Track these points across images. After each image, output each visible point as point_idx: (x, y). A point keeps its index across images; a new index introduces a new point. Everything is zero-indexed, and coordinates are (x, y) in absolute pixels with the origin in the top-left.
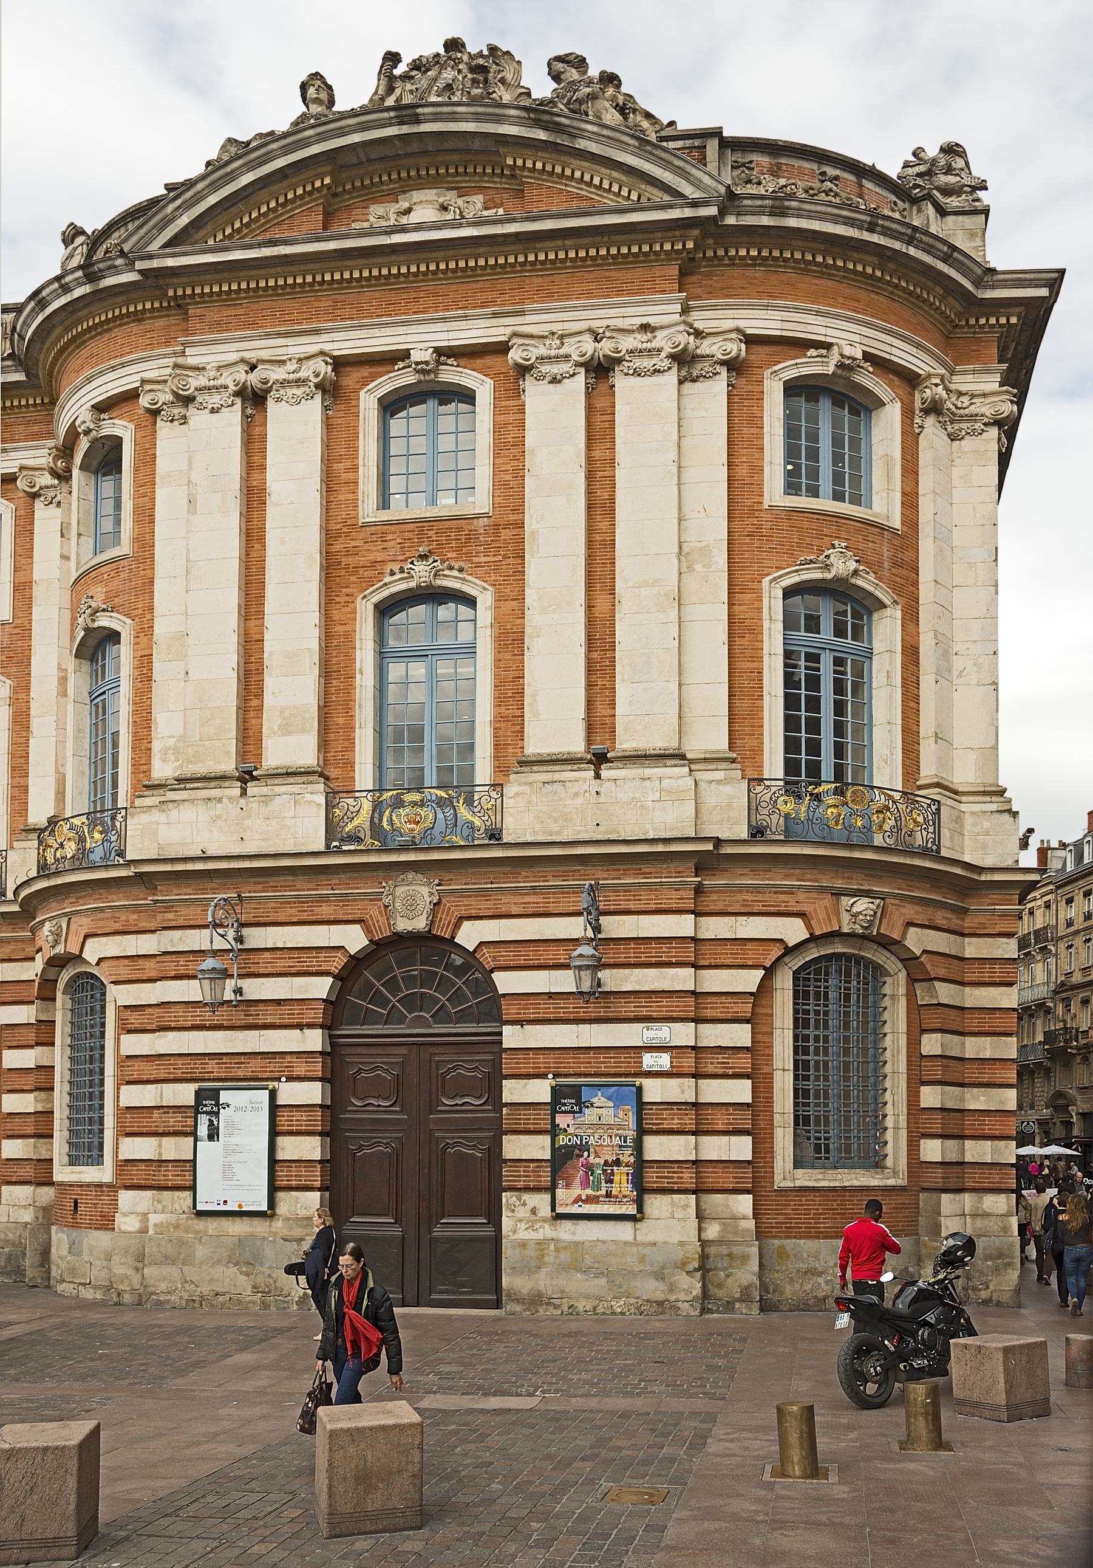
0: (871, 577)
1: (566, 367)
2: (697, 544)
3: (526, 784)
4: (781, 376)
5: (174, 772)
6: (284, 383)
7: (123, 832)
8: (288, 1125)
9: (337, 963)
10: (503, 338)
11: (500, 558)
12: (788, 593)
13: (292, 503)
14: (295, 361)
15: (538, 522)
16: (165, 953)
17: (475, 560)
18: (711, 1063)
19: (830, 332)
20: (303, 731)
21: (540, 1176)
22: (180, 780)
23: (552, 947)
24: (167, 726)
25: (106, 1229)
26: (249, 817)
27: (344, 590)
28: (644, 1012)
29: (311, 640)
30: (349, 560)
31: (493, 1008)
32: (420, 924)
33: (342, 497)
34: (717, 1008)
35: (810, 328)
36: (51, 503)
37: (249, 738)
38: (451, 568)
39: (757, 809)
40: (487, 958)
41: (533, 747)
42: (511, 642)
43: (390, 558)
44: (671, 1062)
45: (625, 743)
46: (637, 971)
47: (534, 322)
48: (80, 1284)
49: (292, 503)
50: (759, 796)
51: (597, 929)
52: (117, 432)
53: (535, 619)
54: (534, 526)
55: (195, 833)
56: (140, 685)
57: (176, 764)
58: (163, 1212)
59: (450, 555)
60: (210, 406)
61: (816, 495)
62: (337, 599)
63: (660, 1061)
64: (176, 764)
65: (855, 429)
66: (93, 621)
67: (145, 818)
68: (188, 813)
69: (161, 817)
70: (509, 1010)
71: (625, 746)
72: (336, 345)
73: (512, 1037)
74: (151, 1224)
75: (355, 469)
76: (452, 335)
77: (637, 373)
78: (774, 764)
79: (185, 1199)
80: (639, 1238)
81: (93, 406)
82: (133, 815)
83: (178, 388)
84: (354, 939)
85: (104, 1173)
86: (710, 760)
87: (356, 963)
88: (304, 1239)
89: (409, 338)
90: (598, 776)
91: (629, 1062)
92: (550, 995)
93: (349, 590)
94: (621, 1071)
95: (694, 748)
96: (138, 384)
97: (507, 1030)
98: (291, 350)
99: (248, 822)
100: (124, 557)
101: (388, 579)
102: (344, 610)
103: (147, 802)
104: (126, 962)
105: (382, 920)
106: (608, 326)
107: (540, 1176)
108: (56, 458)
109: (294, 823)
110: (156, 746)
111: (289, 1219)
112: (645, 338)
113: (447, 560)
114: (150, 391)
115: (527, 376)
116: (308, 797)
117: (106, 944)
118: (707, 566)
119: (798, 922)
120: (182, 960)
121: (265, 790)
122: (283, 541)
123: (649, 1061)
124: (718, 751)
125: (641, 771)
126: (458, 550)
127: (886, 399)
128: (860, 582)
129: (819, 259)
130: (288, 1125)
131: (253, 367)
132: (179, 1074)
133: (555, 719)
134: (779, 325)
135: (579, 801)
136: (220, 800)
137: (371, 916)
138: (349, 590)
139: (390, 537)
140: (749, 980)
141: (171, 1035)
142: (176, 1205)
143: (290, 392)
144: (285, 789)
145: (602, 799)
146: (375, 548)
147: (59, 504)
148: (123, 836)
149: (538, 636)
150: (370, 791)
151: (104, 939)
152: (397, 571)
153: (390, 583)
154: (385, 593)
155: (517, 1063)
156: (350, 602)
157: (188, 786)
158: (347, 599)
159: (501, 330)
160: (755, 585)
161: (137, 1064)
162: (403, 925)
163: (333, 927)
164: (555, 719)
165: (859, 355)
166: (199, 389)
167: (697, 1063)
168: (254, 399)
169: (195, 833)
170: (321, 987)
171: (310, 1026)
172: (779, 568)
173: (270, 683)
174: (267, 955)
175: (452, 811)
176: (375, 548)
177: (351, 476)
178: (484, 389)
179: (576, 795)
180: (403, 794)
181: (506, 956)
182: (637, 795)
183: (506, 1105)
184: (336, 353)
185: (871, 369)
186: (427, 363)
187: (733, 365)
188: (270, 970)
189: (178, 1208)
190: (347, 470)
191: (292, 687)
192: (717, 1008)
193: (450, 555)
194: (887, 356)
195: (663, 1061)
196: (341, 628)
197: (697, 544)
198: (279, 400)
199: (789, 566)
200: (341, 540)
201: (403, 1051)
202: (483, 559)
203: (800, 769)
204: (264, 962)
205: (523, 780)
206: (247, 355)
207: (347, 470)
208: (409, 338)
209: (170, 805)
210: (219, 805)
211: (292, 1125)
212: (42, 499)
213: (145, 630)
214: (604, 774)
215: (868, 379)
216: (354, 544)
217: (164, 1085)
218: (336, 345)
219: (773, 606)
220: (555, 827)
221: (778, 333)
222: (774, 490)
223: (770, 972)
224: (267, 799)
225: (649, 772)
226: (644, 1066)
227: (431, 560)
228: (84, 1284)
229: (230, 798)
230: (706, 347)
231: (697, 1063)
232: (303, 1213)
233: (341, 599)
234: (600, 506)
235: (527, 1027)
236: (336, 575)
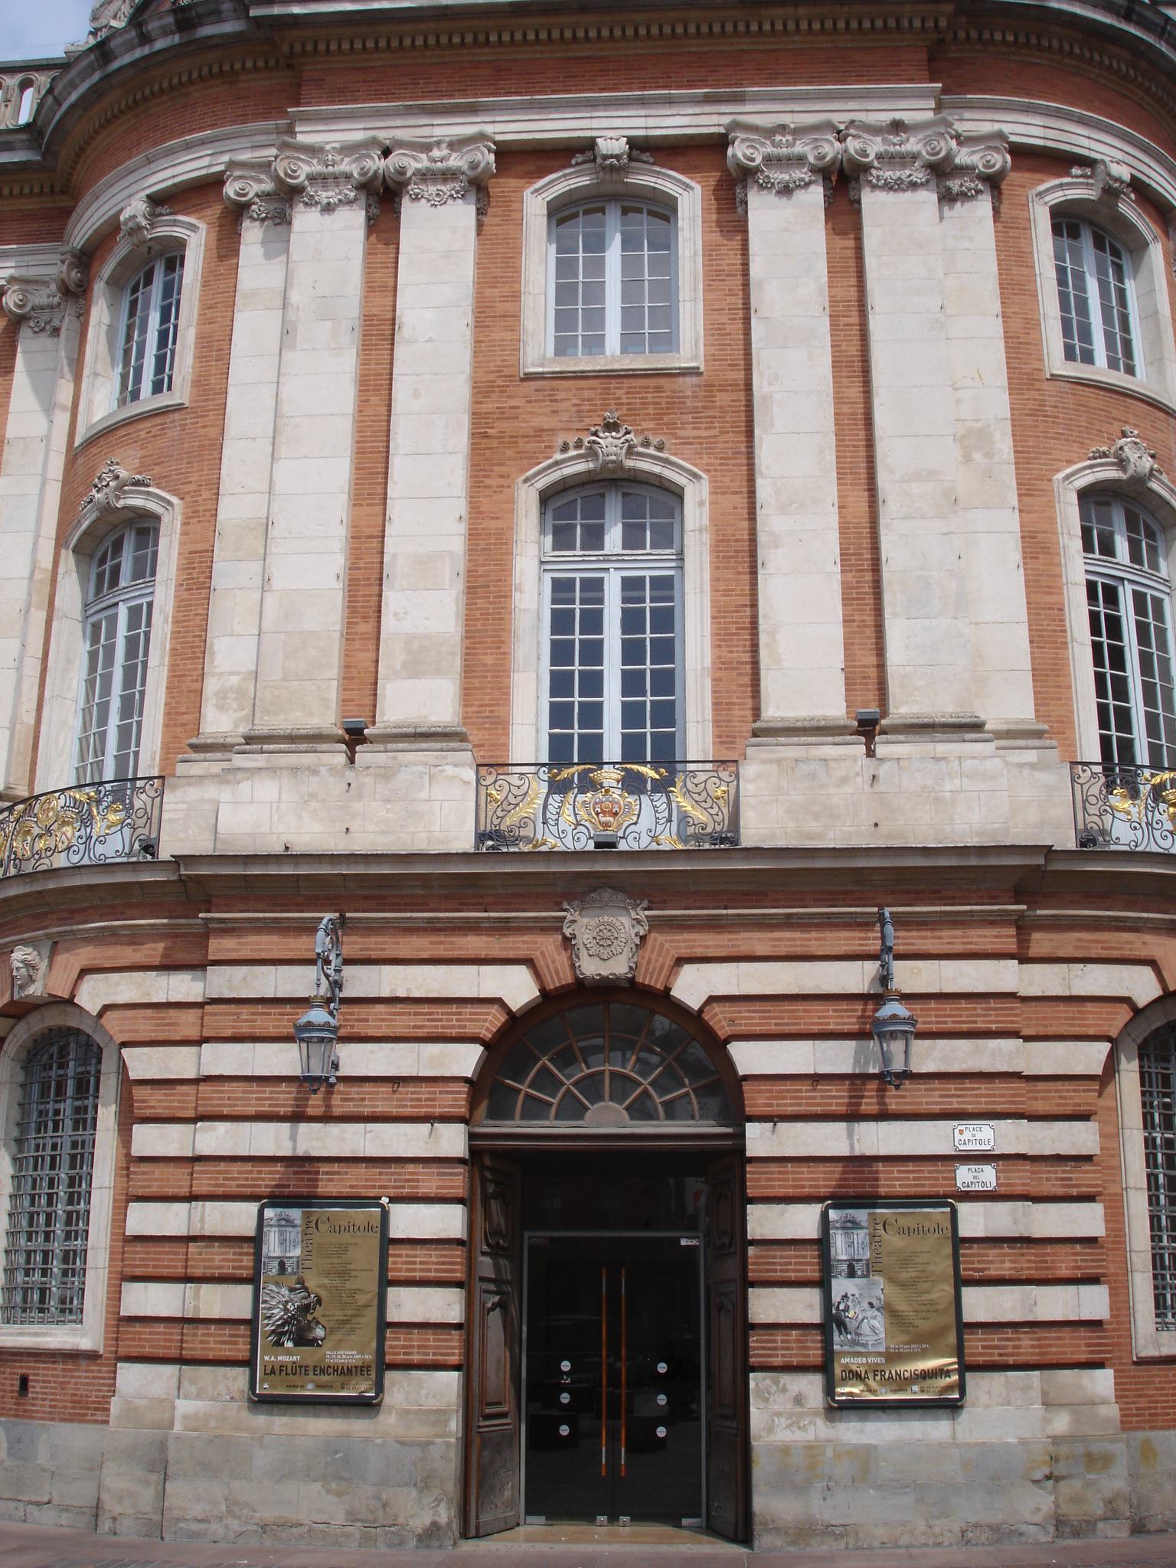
1: (800, 174)
2: (975, 425)
3: (771, 761)
4: (1047, 199)
5: (236, 726)
6: (425, 176)
7: (156, 813)
8: (407, 1270)
9: (490, 1022)
10: (722, 130)
11: (715, 432)
12: (1084, 495)
13: (431, 340)
14: (444, 146)
15: (770, 384)
16: (214, 1001)
17: (680, 433)
18: (1048, 1180)
19: (1094, 145)
20: (438, 672)
21: (807, 1348)
22: (249, 739)
23: (817, 1006)
24: (229, 656)
25: (80, 1422)
26: (360, 797)
27: (496, 469)
28: (955, 1105)
29: (453, 540)
30: (505, 425)
31: (728, 1094)
32: (618, 967)
33: (496, 336)
34: (1053, 1098)
35: (1074, 139)
36: (43, 330)
37: (362, 679)
38: (646, 444)
39: (1085, 809)
40: (720, 1021)
41: (774, 710)
42: (742, 555)
43: (561, 425)
44: (998, 1178)
45: (903, 707)
46: (941, 1043)
47: (759, 113)
48: (30, 1503)
49: (431, 340)
50: (1085, 787)
52: (179, 232)
53: (771, 522)
54: (766, 389)
55: (275, 818)
56: (186, 595)
57: (239, 714)
58: (198, 1397)
59: (645, 425)
60: (325, 201)
62: (488, 482)
63: (982, 1177)
64: (239, 714)
65: (657, 265)
66: (118, 498)
67: (192, 793)
68: (266, 790)
69: (225, 794)
70: (756, 1100)
71: (903, 710)
72: (499, 128)
73: (758, 1139)
74: (178, 1414)
75: (516, 296)
76: (651, 122)
77: (888, 187)
79: (235, 1379)
80: (454, 1359)
81: (148, 196)
82: (174, 788)
83: (286, 174)
84: (517, 988)
85: (85, 1335)
86: (1012, 735)
87: (516, 1022)
88: (432, 1443)
89: (595, 123)
90: (870, 753)
91: (937, 1179)
92: (816, 1078)
93: (504, 470)
94: (931, 1190)
95: (994, 717)
96: (222, 168)
97: (752, 1130)
98: (438, 132)
99: (358, 806)
100: (179, 408)
101: (559, 456)
102: (496, 497)
103: (196, 769)
104: (149, 1012)
105: (561, 959)
106: (853, 122)
107: (807, 1348)
108: (72, 266)
109: (432, 812)
110: (211, 686)
111: (407, 1412)
112: (896, 140)
113: (642, 431)
114: (240, 177)
115: (750, 181)
116: (450, 770)
117: (118, 984)
118: (989, 455)
119: (1147, 972)
120: (245, 1011)
121: (382, 758)
122: (416, 394)
123: (965, 1176)
124: (1023, 721)
125: (930, 746)
126: (657, 418)
127: (1149, 238)
128: (1154, 485)
129: (1077, 50)
130: (407, 1270)
131: (386, 153)
132: (232, 1188)
133: (805, 671)
134: (1040, 132)
135: (848, 789)
136: (315, 772)
137: (542, 953)
138: (504, 470)
139: (561, 396)
141: (222, 1127)
142: (221, 1388)
143: (432, 189)
144: (415, 760)
145: (880, 787)
146: (541, 411)
147: (56, 331)
148: (155, 820)
149: (777, 547)
150: (543, 765)
151: (116, 976)
152: (571, 445)
153: (563, 461)
154: (555, 476)
155: (768, 1179)
156: (505, 485)
157: (265, 747)
158: (502, 481)
159: (715, 119)
160: (1044, 485)
161: (158, 1170)
162: (591, 968)
163: (484, 969)
164: (805, 671)
165: (1127, 178)
166: (312, 178)
167: (1031, 1178)
168: (383, 199)
169: (275, 818)
170: (465, 1060)
171: (445, 1119)
172: (1070, 462)
173: (393, 599)
174: (380, 1008)
175: (664, 799)
176: (541, 411)
177: (508, 307)
178: (691, 198)
179: (844, 780)
180: (592, 771)
181: (749, 1018)
182: (930, 783)
183: (753, 1242)
184: (499, 138)
185: (1133, 196)
186: (618, 157)
187: (993, 182)
188: (383, 1031)
189: (224, 1392)
190: (504, 299)
191: (424, 609)
192: (1053, 1098)
193: (645, 425)
194: (1147, 180)
195: (987, 1177)
196: (493, 524)
197: (975, 425)
198: (416, 198)
199: (1081, 460)
200: (495, 397)
202: (690, 433)
204: (376, 1020)
205: (764, 756)
206: (382, 135)
207: (504, 299)
208: (595, 123)
209: (240, 775)
210: (314, 779)
211: (414, 1270)
212: (32, 324)
213: (204, 512)
214: (881, 750)
215: (1128, 209)
216: (512, 403)
217: (208, 1204)
218: (499, 128)
219: (1069, 516)
220: (814, 826)
221: (1041, 142)
222: (1055, 361)
224: (386, 774)
225: (942, 748)
226: (959, 1184)
227: (623, 431)
228: (38, 1504)
229: (332, 769)
230: (964, 156)
231: (1031, 1178)
232: (430, 1403)
233: (493, 482)
235: (783, 1126)
236: (492, 448)
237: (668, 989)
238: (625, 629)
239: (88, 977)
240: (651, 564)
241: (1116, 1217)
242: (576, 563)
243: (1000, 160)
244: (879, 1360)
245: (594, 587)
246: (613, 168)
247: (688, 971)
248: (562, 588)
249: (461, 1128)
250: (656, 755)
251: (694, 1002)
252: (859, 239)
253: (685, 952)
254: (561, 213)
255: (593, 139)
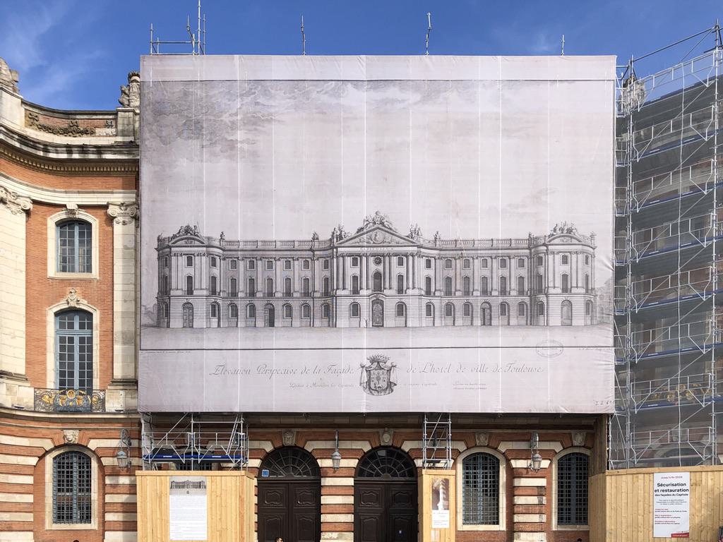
0: (85, 302)
51: (130, 444)
61: (73, 271)
78: (52, 381)
119: (49, 441)
140: (33, 461)
170: (353, 463)
171: (350, 477)
201: (381, 486)
203: (65, 382)
215: (82, 215)
222: (52, 270)
223: (42, 458)
234: (413, 274)
237: (400, 447)
239: (308, 442)
240: (85, 333)
243: (29, 206)
245: (71, 340)
246: (72, 212)
247: (92, 441)
248: (62, 340)
249: (353, 479)
251: (310, 450)
253: (91, 436)
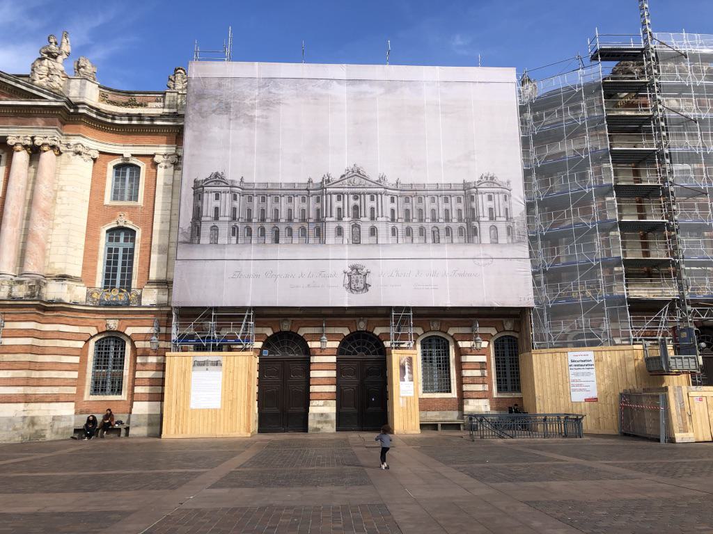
84: (346, 332)
119: (95, 328)
170: (336, 344)
238: (123, 258)
240: (129, 245)
241: (489, 359)
242: (114, 245)
244: (604, 360)
245: (117, 250)
247: (128, 328)
248: (110, 250)
250: (126, 284)
251: (377, 334)
252: (157, 170)
254: (117, 167)
255: (477, 235)
